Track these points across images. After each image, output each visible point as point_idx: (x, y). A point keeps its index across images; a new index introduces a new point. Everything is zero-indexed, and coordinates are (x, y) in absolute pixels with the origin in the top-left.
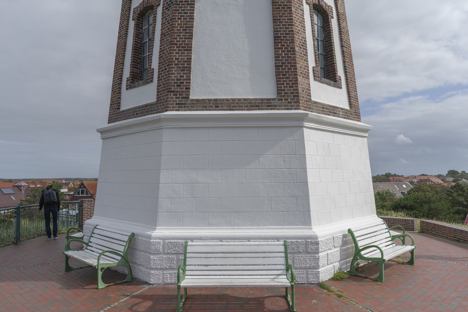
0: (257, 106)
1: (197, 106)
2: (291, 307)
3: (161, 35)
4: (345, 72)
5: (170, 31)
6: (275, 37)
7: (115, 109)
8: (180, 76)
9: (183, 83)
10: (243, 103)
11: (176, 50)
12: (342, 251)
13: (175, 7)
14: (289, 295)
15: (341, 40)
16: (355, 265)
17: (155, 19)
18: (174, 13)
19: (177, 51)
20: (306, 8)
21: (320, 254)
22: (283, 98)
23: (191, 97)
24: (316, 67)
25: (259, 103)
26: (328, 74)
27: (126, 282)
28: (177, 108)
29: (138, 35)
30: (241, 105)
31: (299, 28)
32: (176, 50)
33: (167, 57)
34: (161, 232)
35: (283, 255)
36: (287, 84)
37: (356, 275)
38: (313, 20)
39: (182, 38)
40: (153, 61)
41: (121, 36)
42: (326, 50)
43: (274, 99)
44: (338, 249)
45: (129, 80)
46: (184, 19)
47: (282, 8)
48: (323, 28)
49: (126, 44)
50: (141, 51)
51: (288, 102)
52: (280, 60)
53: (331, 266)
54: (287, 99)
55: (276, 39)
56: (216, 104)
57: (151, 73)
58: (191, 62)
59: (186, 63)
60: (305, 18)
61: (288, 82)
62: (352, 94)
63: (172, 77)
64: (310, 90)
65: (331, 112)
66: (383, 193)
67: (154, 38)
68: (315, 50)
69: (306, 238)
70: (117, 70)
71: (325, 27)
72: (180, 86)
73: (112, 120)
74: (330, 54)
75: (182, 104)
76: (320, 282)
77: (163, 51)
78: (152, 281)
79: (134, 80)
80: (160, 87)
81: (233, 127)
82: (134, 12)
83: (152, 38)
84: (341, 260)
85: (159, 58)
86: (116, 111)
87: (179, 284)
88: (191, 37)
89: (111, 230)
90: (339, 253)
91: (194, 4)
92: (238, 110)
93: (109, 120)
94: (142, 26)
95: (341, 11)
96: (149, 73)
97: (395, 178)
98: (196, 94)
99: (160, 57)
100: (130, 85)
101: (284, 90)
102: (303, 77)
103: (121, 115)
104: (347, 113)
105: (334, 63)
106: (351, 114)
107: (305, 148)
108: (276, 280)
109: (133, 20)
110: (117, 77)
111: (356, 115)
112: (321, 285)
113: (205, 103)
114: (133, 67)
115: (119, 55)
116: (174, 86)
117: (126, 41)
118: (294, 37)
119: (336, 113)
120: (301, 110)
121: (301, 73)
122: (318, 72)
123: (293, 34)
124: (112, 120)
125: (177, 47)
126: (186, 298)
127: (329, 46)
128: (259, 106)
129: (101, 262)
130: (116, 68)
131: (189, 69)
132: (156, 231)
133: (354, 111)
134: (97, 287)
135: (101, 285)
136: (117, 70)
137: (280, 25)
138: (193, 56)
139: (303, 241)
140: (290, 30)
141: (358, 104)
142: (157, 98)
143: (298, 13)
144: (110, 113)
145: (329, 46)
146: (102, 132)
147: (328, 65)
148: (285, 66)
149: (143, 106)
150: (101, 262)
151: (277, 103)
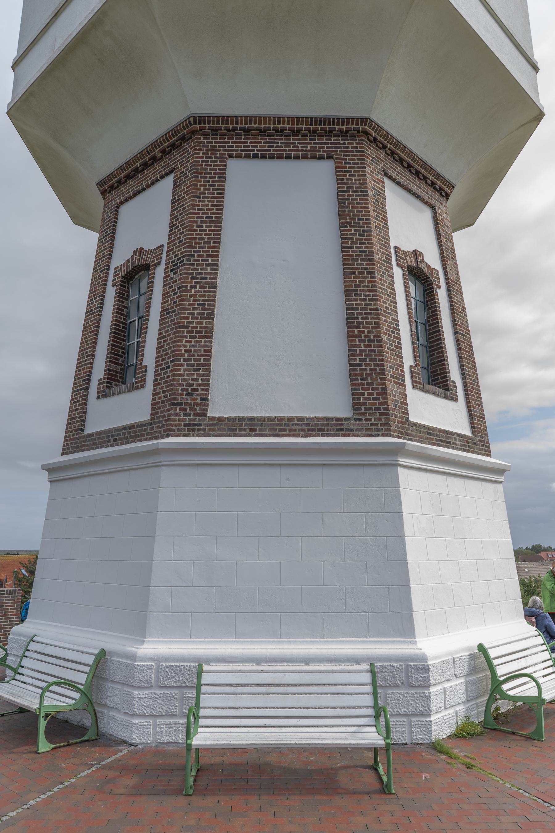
0: (319, 430)
1: (219, 429)
2: (386, 786)
3: (161, 312)
5: (177, 306)
7: (76, 430)
8: (193, 379)
9: (197, 390)
10: (296, 424)
11: (186, 337)
12: (468, 684)
13: (185, 269)
14: (380, 764)
15: (454, 322)
16: (492, 710)
17: (151, 285)
18: (184, 278)
19: (188, 339)
20: (398, 273)
21: (432, 690)
23: (210, 414)
24: (416, 365)
25: (322, 425)
26: (435, 378)
27: (87, 741)
28: (186, 432)
29: (121, 311)
30: (292, 428)
31: (387, 305)
32: (186, 337)
34: (154, 648)
35: (369, 689)
36: (369, 394)
37: (495, 729)
38: (409, 292)
39: (197, 318)
42: (430, 338)
43: (347, 419)
44: (462, 680)
45: (103, 383)
46: (200, 287)
47: (359, 273)
48: (424, 303)
50: (124, 336)
51: (372, 425)
53: (451, 711)
56: (252, 426)
57: (142, 372)
58: (210, 356)
59: (202, 358)
60: (396, 288)
61: (371, 391)
62: (475, 411)
63: (179, 380)
65: (441, 441)
66: (530, 582)
67: (148, 315)
68: (412, 339)
69: (406, 659)
70: (82, 366)
71: (427, 301)
72: (191, 395)
73: (69, 449)
74: (437, 345)
75: (194, 425)
76: (434, 740)
77: (164, 337)
78: (136, 738)
79: (111, 383)
82: (115, 273)
84: (468, 701)
85: (158, 348)
86: (78, 434)
87: (189, 742)
88: (211, 317)
89: (62, 645)
90: (463, 687)
92: (289, 436)
93: (63, 450)
94: (128, 296)
95: (452, 277)
96: (139, 373)
97: (549, 553)
98: (216, 409)
99: (159, 347)
100: (103, 391)
101: (365, 404)
102: (395, 383)
103: (85, 441)
104: (467, 442)
106: (475, 444)
107: (401, 502)
108: (359, 735)
109: (113, 285)
111: (482, 445)
112: (436, 747)
114: (110, 362)
115: (87, 341)
116: (182, 395)
117: (100, 320)
118: (378, 319)
119: (450, 443)
120: (393, 436)
121: (392, 377)
122: (419, 374)
123: (378, 314)
124: (69, 449)
125: (188, 332)
126: (198, 770)
127: (435, 332)
128: (324, 430)
129: (45, 703)
131: (208, 367)
132: (145, 646)
133: (478, 441)
134: (35, 749)
135: (44, 746)
136: (82, 366)
137: (356, 300)
138: (215, 347)
139: (401, 665)
140: (372, 307)
141: (485, 427)
142: (152, 414)
143: (384, 281)
144: (65, 437)
145: (435, 332)
146: (51, 469)
147: (434, 363)
148: (366, 365)
149: (125, 428)
150: (45, 703)
151: (352, 424)
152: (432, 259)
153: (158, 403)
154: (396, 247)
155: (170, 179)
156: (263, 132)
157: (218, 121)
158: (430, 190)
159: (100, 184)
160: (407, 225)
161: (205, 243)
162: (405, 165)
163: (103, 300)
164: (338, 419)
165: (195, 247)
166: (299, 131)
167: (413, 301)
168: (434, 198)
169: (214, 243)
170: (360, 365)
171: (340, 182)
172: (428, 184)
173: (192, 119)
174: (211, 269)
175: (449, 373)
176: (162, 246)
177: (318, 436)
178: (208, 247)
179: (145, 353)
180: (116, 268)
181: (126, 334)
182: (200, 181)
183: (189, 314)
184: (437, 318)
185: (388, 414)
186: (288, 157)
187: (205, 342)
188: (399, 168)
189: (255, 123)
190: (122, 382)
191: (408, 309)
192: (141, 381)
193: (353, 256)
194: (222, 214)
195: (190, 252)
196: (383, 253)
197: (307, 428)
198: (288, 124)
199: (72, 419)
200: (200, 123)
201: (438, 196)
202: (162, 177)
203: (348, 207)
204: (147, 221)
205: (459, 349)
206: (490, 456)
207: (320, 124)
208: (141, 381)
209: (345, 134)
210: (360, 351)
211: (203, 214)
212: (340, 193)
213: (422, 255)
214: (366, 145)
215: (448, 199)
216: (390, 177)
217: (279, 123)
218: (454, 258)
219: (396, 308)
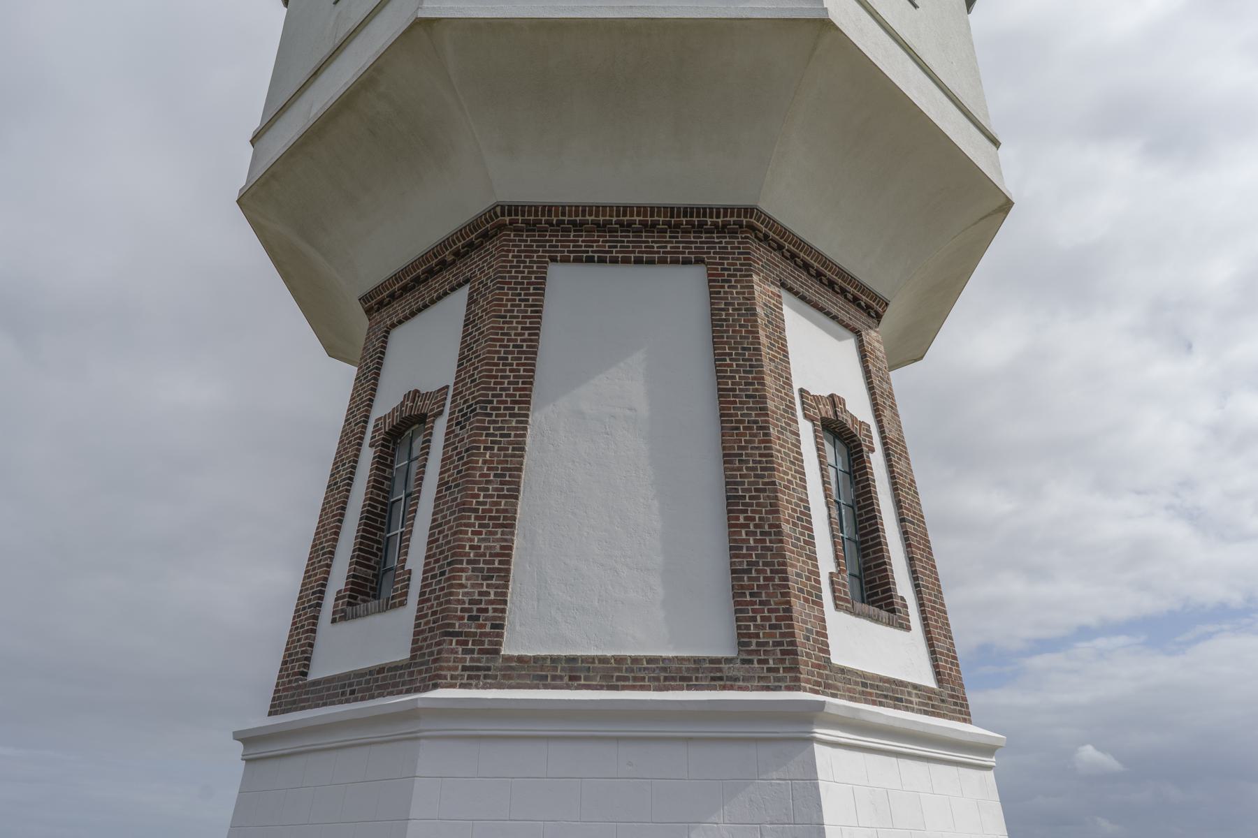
0: (683, 679)
1: (519, 677)
5: (462, 477)
7: (295, 674)
8: (481, 594)
9: (486, 610)
10: (645, 669)
13: (478, 421)
18: (476, 435)
19: (477, 528)
20: (806, 429)
23: (505, 651)
25: (688, 669)
26: (871, 592)
28: (465, 681)
36: (763, 619)
38: (825, 457)
39: (492, 496)
42: (862, 529)
43: (729, 660)
45: (344, 597)
46: (499, 449)
47: (745, 428)
50: (382, 523)
51: (769, 670)
56: (573, 671)
57: (404, 580)
58: (510, 556)
60: (803, 451)
62: (941, 646)
63: (458, 594)
65: (886, 697)
67: (419, 492)
68: (832, 530)
73: (280, 705)
75: (478, 669)
77: (440, 525)
79: (355, 598)
85: (429, 543)
86: (297, 680)
92: (633, 688)
93: (272, 706)
94: (392, 462)
95: (892, 434)
100: (342, 611)
101: (757, 635)
102: (806, 600)
103: (307, 693)
104: (930, 698)
106: (943, 701)
107: (820, 806)
109: (371, 446)
111: (955, 704)
114: (357, 563)
116: (462, 618)
118: (776, 498)
119: (901, 700)
120: (805, 690)
121: (801, 590)
122: (844, 586)
124: (280, 705)
125: (477, 518)
128: (690, 679)
131: (505, 574)
137: (740, 469)
138: (517, 542)
142: (413, 650)
146: (248, 739)
147: (870, 568)
148: (758, 571)
149: (371, 672)
151: (737, 670)
152: (859, 408)
153: (423, 632)
154: (801, 390)
155: (464, 292)
156: (601, 227)
157: (536, 211)
158: (853, 309)
159: (364, 299)
160: (817, 358)
161: (509, 383)
162: (813, 272)
163: (354, 468)
164: (713, 661)
165: (495, 389)
166: (654, 224)
167: (832, 472)
168: (859, 319)
169: (523, 383)
170: (749, 571)
171: (714, 295)
172: (849, 301)
173: (498, 210)
174: (518, 422)
175: (894, 583)
176: (447, 387)
177: (681, 688)
178: (515, 389)
179: (410, 551)
180: (377, 420)
181: (386, 521)
182: (507, 294)
183: (479, 489)
184: (871, 498)
185: (795, 653)
186: (638, 261)
187: (503, 534)
188: (804, 276)
189: (590, 215)
190: (374, 597)
191: (824, 483)
192: (401, 595)
193: (735, 402)
194: (537, 341)
195: (487, 395)
196: (782, 398)
197: (663, 674)
198: (638, 215)
199: (290, 655)
200: (510, 215)
201: (864, 317)
202: (453, 289)
203: (727, 331)
204: (427, 352)
205: (908, 545)
206: (970, 722)
207: (685, 216)
208: (401, 595)
209: (722, 229)
210: (748, 548)
211: (509, 340)
212: (715, 314)
213: (842, 401)
214: (753, 245)
215: (879, 322)
216: (790, 290)
217: (625, 215)
218: (893, 407)
219: (805, 481)
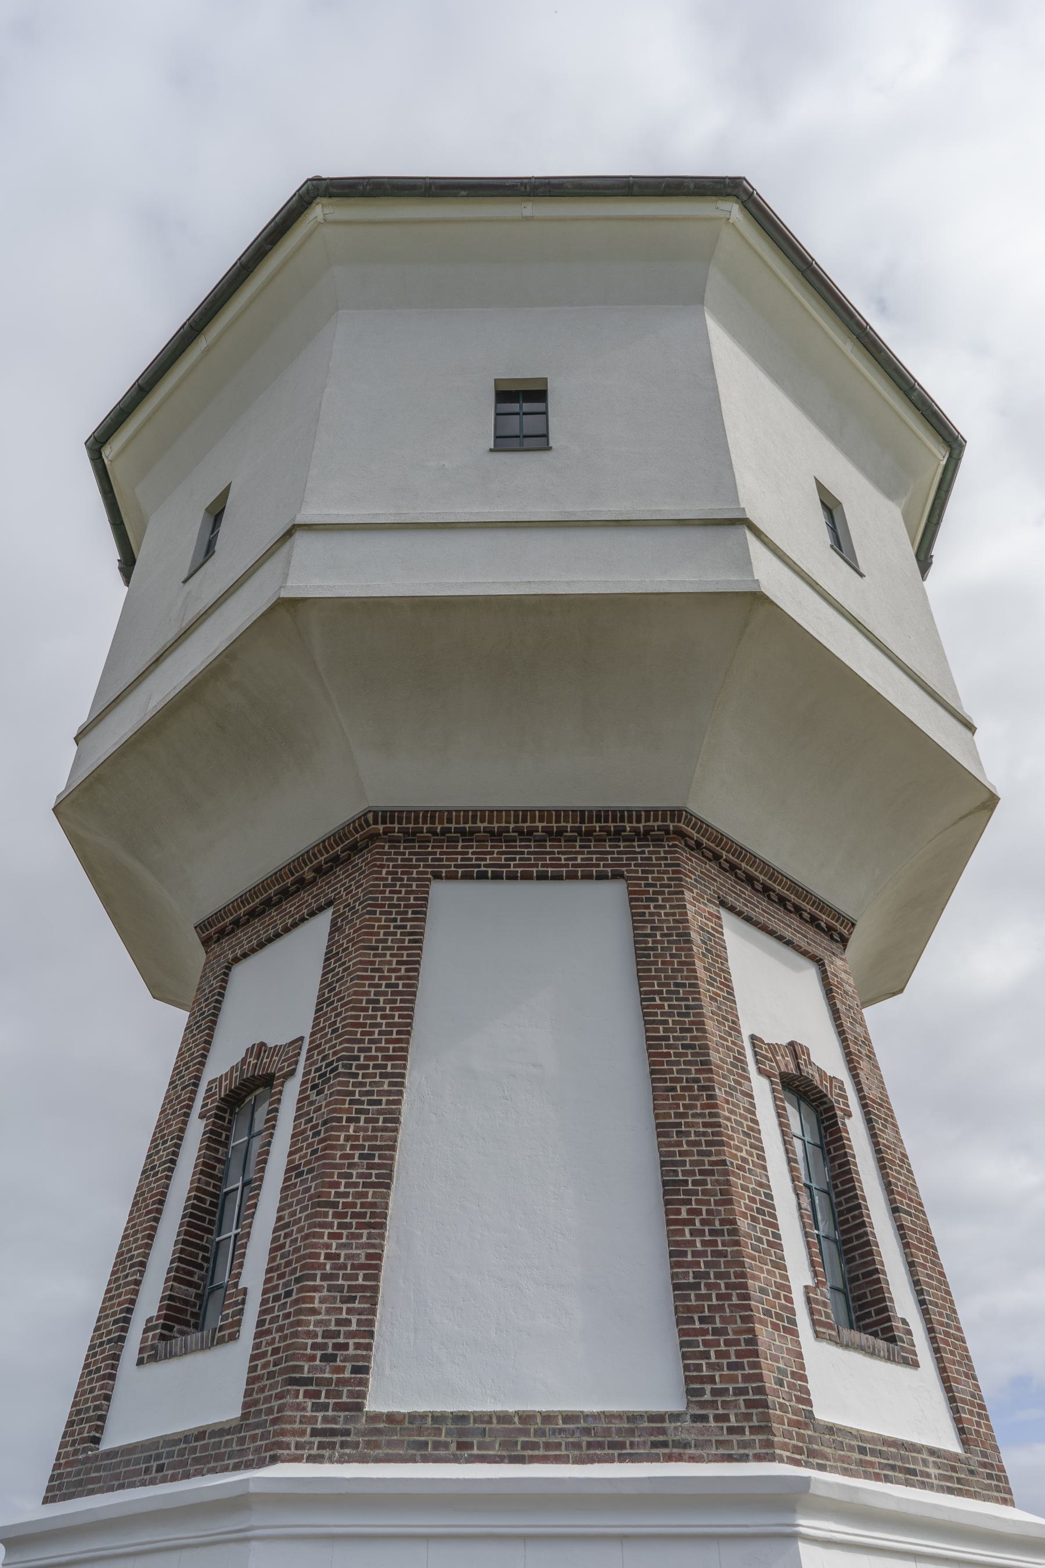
0: (613, 1445)
1: (390, 1444)
3: (287, 1171)
4: (922, 1303)
5: (317, 1159)
6: (665, 1183)
7: (83, 1440)
8: (339, 1323)
9: (345, 1347)
10: (561, 1431)
11: (330, 1225)
13: (340, 1084)
18: (336, 1102)
19: (335, 1230)
20: (761, 1088)
22: (711, 1413)
23: (371, 1406)
25: (619, 1431)
26: (862, 1312)
28: (314, 1452)
29: (211, 1169)
31: (744, 1154)
32: (330, 1225)
33: (297, 1250)
36: (719, 1355)
38: (788, 1126)
39: (355, 1185)
40: (249, 1251)
41: (153, 1168)
42: (842, 1223)
43: (675, 1417)
45: (155, 1327)
46: (367, 1121)
47: (683, 1089)
48: (821, 1147)
49: (164, 1194)
51: (731, 1430)
52: (690, 1265)
54: (725, 1418)
55: (672, 1189)
57: (236, 1304)
58: (378, 1267)
59: (361, 1273)
61: (723, 1348)
62: (962, 1390)
64: (804, 1378)
65: (893, 1468)
67: (261, 1179)
68: (804, 1226)
70: (118, 1288)
71: (828, 1144)
73: (60, 1487)
75: (333, 1433)
77: (287, 1225)
79: (170, 1329)
80: (260, 1363)
81: (525, 1538)
83: (256, 1180)
86: (85, 1450)
88: (385, 1183)
91: (403, 1076)
93: (49, 1489)
94: (228, 1138)
95: (872, 1093)
96: (229, 1306)
100: (153, 1347)
102: (775, 1327)
103: (98, 1469)
104: (954, 1469)
105: (876, 1271)
106: (972, 1472)
109: (201, 1116)
110: (114, 1314)
111: (990, 1476)
113: (420, 1431)
115: (136, 1232)
116: (312, 1358)
118: (728, 1182)
119: (913, 1472)
121: (767, 1313)
122: (825, 1304)
125: (336, 1215)
127: (850, 1210)
130: (117, 1279)
133: (977, 1467)
136: (118, 1288)
137: (679, 1144)
138: (390, 1249)
140: (714, 1158)
141: (989, 1428)
142: (245, 1405)
143: (734, 1104)
145: (850, 1210)
149: (186, 1437)
151: (687, 1430)
